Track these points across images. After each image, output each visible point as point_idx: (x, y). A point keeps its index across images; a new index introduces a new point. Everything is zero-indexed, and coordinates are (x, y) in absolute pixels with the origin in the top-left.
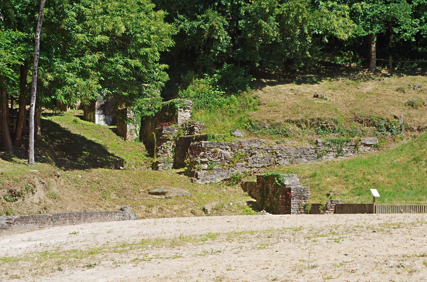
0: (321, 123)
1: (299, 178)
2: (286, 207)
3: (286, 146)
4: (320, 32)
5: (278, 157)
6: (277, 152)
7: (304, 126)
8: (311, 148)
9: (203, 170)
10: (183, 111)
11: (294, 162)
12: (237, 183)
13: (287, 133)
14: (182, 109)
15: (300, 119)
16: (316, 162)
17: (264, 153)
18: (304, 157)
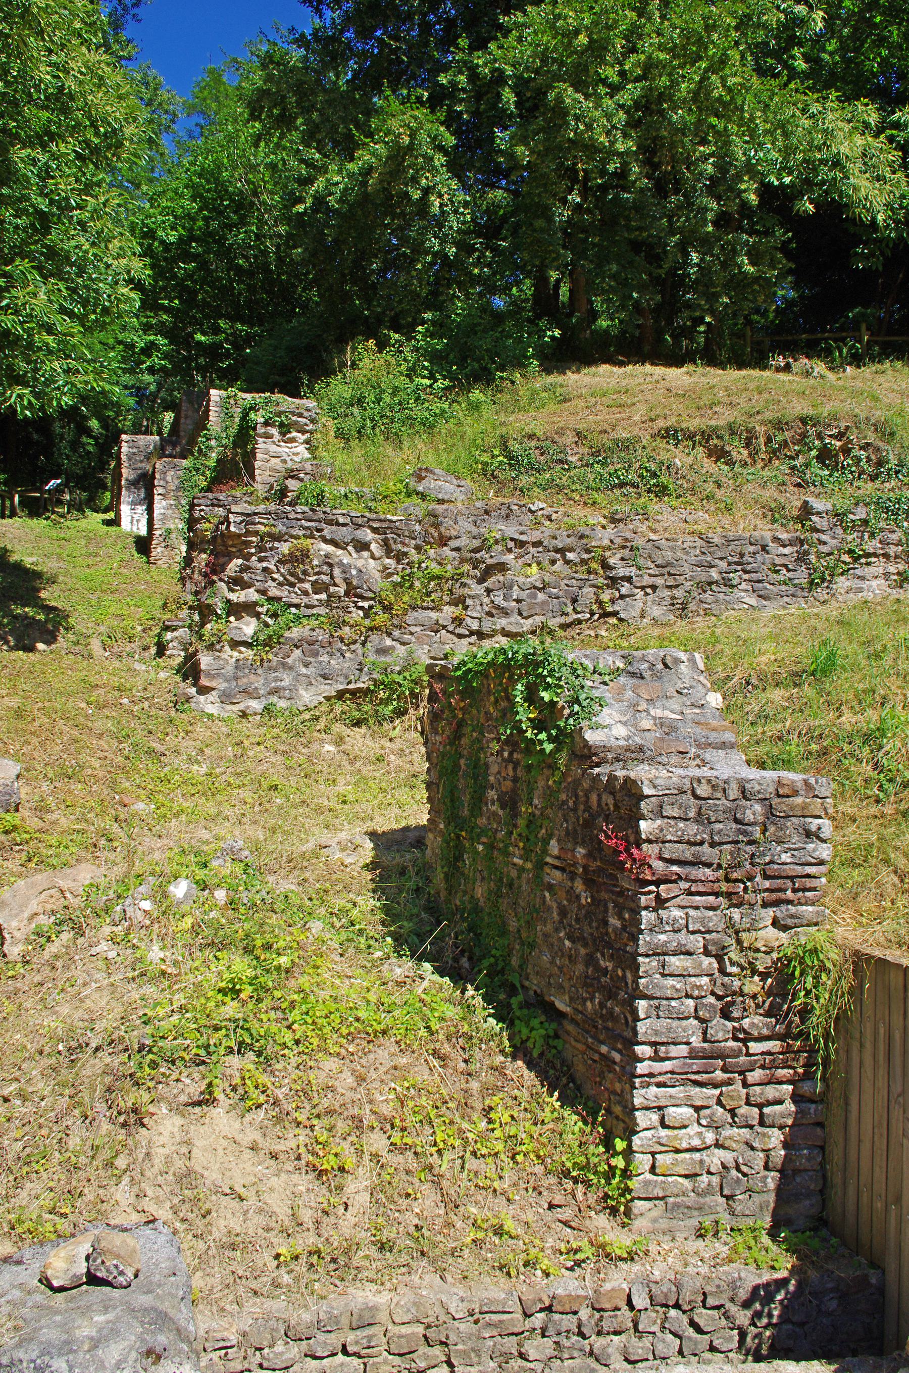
0: (820, 436)
1: (718, 685)
2: (590, 960)
3: (655, 531)
4: (787, 180)
5: (614, 582)
6: (612, 561)
7: (740, 453)
8: (776, 539)
9: (235, 644)
10: (277, 436)
11: (692, 606)
12: (400, 713)
13: (663, 480)
14: (274, 431)
15: (722, 423)
16: (798, 608)
17: (546, 563)
18: (744, 586)
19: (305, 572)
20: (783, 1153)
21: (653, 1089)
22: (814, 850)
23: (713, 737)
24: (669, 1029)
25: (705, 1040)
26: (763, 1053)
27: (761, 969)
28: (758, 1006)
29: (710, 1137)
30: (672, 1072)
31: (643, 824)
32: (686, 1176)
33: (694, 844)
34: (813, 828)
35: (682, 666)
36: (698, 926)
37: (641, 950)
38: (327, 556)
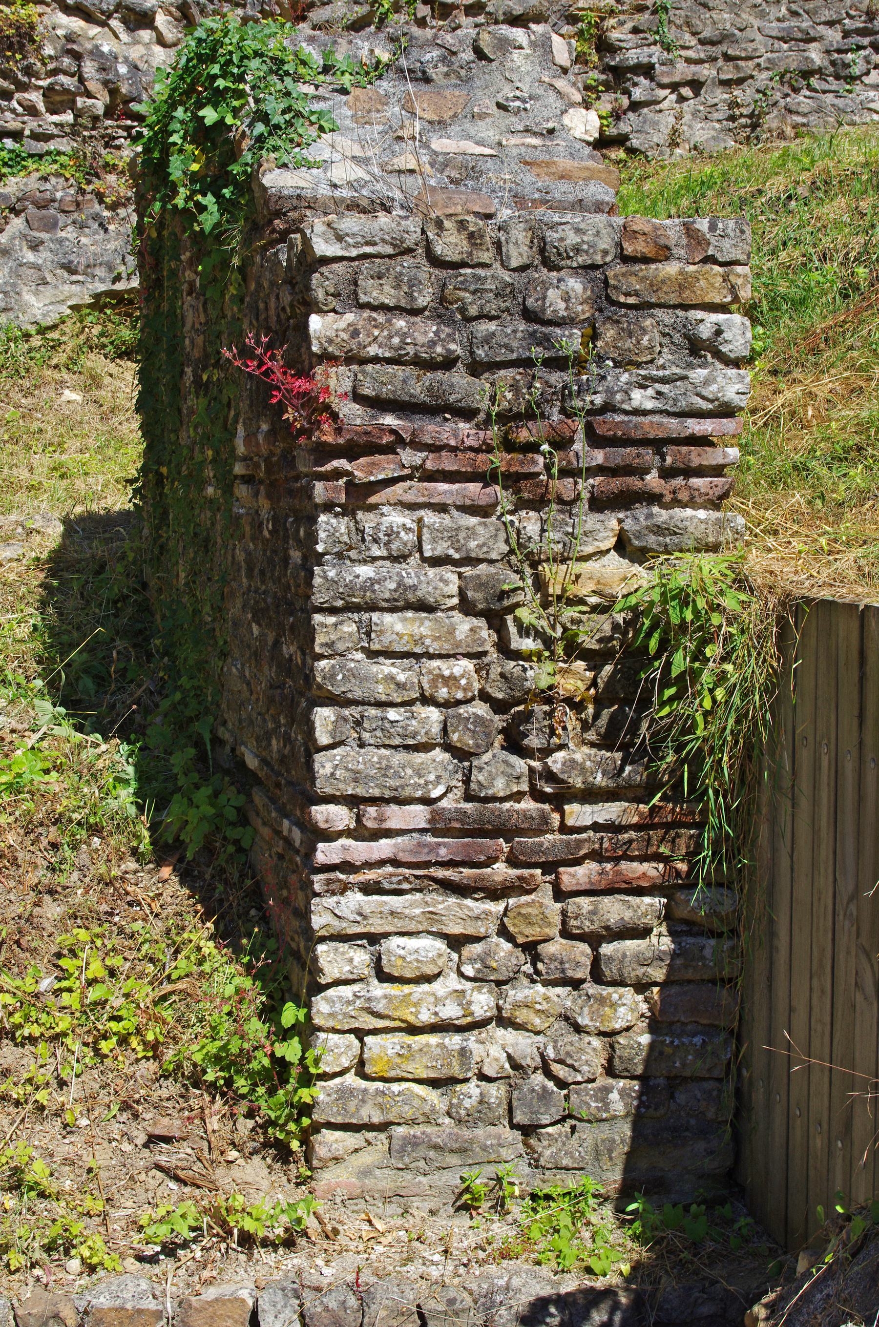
11: (771, 121)
19: (28, 71)
20: (645, 1039)
21: (355, 898)
22: (706, 382)
23: (561, 190)
24: (385, 770)
25: (468, 797)
26: (596, 827)
27: (591, 644)
28: (586, 726)
29: (482, 1002)
30: (395, 862)
31: (315, 322)
32: (433, 1083)
33: (430, 365)
34: (705, 332)
35: (516, 55)
36: (442, 548)
37: (319, 598)
38: (70, 38)
